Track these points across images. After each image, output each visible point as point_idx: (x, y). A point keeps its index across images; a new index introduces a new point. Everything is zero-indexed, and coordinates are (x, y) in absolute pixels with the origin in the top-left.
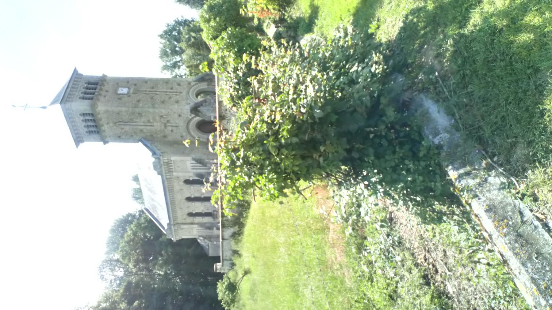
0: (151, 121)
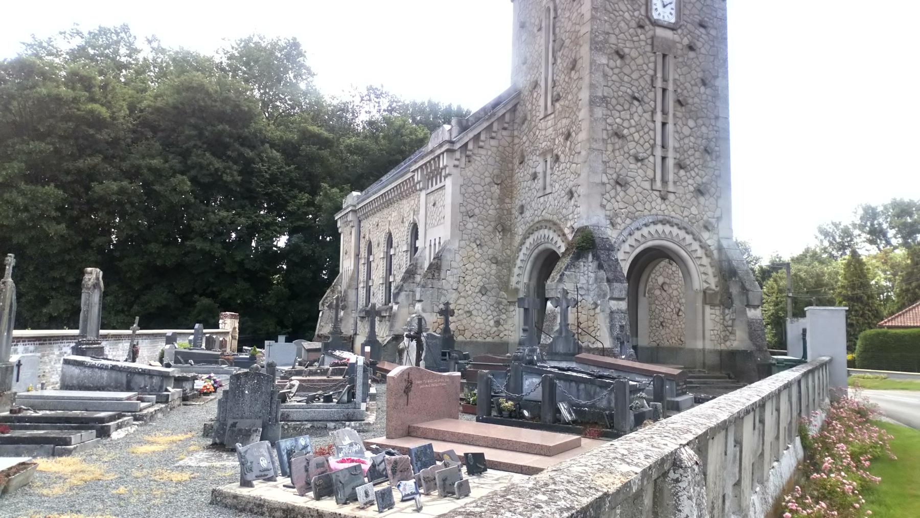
0: (558, 105)
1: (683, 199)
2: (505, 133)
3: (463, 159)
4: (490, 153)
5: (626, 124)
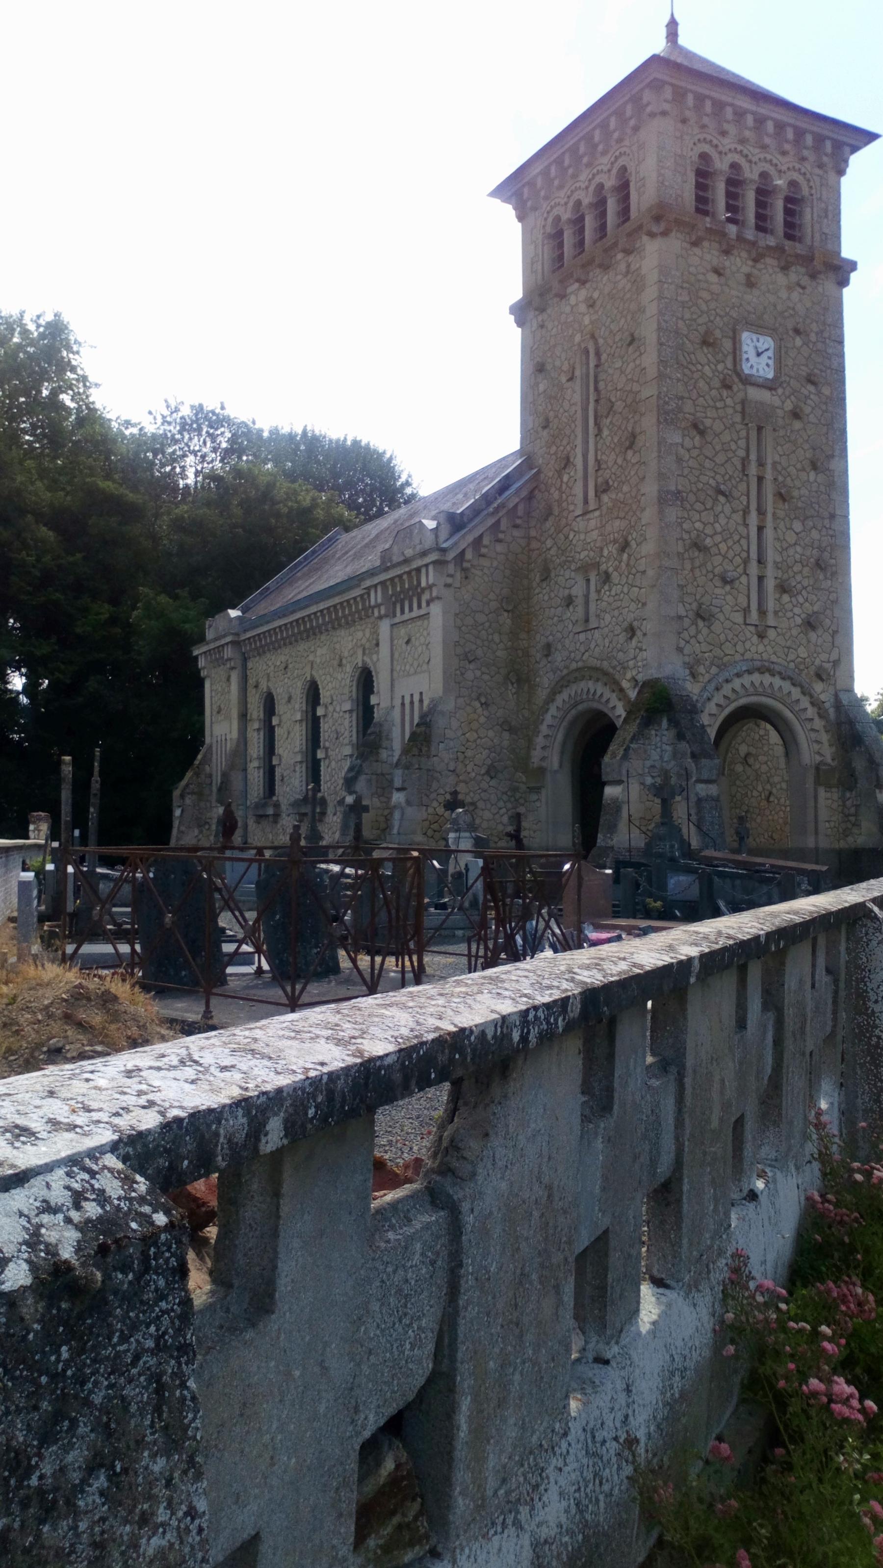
0: (605, 498)
1: (787, 636)
2: (516, 533)
3: (458, 575)
4: (495, 564)
5: (709, 531)
